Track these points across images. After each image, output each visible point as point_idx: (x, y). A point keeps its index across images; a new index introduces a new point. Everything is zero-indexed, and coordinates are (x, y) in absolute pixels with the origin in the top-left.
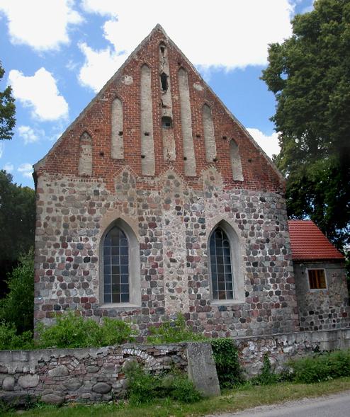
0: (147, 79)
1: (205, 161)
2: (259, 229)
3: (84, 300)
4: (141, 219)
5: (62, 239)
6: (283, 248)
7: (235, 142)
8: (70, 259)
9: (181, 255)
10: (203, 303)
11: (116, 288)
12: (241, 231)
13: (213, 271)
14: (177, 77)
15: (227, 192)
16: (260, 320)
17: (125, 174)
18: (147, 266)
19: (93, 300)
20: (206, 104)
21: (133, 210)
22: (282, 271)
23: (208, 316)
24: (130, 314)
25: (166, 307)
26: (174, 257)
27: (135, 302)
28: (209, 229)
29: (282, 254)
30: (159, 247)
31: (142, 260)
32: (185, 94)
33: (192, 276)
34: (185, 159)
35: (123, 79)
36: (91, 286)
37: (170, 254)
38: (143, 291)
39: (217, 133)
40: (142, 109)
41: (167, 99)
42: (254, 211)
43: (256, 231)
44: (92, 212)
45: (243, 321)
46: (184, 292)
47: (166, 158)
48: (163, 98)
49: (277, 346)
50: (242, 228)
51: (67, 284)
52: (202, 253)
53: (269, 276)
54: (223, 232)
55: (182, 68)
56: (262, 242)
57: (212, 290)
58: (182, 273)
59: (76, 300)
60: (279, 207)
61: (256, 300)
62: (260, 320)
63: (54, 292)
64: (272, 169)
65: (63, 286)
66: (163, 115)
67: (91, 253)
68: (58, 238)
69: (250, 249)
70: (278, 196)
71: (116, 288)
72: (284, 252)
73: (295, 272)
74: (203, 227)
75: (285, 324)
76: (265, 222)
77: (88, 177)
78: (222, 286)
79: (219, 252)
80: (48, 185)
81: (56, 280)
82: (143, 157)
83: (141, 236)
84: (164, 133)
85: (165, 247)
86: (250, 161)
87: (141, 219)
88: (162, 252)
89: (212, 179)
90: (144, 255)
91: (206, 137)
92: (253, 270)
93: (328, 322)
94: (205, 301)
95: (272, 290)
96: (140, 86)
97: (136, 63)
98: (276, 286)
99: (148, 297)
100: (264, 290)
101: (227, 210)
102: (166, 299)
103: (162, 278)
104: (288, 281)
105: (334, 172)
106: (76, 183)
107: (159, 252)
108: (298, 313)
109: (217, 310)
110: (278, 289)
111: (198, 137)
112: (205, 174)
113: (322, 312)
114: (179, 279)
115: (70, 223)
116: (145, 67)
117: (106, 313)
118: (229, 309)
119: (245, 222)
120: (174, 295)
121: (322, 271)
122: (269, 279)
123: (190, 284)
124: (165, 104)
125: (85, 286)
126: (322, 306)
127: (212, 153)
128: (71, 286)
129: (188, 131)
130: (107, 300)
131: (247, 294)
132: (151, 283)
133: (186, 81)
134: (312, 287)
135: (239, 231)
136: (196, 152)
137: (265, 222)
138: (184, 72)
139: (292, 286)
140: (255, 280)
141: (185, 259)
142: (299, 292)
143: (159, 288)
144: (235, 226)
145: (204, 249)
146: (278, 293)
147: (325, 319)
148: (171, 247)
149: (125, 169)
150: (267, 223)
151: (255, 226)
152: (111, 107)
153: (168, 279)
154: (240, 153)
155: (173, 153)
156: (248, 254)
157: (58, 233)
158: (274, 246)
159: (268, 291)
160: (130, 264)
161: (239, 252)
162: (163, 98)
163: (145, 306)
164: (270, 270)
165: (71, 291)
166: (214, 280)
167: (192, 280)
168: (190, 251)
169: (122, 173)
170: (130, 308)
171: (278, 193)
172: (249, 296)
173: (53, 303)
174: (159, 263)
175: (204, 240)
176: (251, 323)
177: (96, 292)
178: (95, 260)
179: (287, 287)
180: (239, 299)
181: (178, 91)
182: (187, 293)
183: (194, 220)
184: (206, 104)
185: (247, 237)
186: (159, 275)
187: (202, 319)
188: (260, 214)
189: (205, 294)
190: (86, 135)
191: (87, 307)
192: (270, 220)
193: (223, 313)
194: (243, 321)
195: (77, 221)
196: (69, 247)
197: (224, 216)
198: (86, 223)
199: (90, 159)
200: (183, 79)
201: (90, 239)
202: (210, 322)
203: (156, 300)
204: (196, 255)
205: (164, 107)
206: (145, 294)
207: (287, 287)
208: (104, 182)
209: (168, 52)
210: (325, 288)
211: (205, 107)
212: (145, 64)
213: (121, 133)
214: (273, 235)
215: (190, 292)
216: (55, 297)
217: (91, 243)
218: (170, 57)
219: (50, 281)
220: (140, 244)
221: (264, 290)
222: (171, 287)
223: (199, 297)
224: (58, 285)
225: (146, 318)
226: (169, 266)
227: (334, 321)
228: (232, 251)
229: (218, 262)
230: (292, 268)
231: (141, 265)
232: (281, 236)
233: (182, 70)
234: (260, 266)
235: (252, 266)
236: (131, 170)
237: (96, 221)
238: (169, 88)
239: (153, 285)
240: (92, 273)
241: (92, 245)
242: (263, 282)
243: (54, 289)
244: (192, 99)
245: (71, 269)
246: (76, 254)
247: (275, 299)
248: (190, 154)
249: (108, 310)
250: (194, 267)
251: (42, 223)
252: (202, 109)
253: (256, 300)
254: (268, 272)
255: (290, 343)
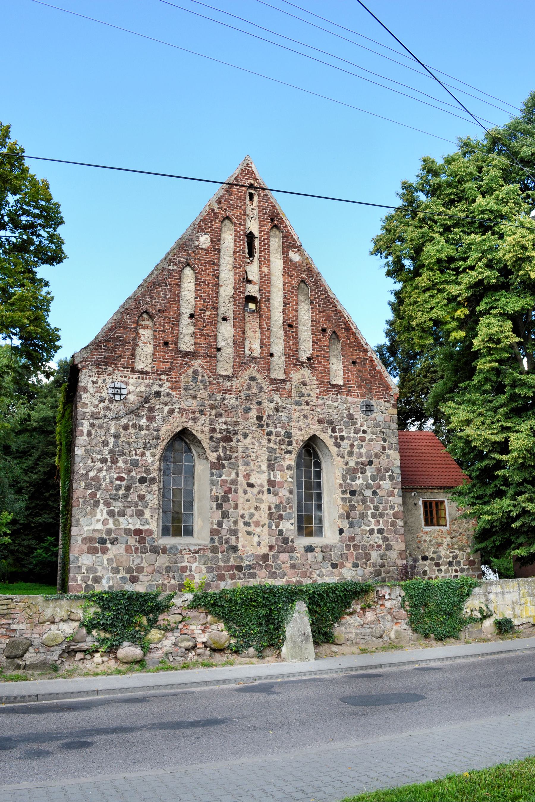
0: (228, 239)
1: (297, 360)
2: (360, 447)
3: (138, 532)
4: (213, 430)
5: (111, 452)
6: (390, 473)
7: (337, 337)
8: (121, 479)
9: (260, 479)
10: (286, 541)
11: (177, 519)
12: (336, 449)
13: (299, 499)
14: (268, 240)
15: (322, 399)
16: (356, 566)
17: (195, 372)
18: (219, 492)
19: (150, 532)
20: (303, 281)
21: (203, 419)
22: (387, 502)
23: (291, 558)
24: (195, 552)
25: (240, 546)
26: (252, 480)
27: (201, 536)
28: (296, 447)
29: (388, 481)
30: (234, 467)
31: (212, 483)
32: (277, 263)
33: (273, 506)
34: (272, 355)
35: (197, 239)
36: (147, 513)
37: (247, 476)
38: (212, 523)
39: (314, 322)
40: (220, 284)
41: (253, 271)
42: (354, 424)
43: (355, 450)
44: (151, 419)
45: (334, 566)
46: (263, 526)
47: (247, 352)
48: (248, 268)
49: (378, 599)
50: (338, 446)
51: (116, 510)
52: (287, 477)
53: (370, 508)
54: (314, 449)
55: (275, 226)
56: (362, 464)
57: (296, 525)
58: (261, 501)
59: (127, 532)
60: (388, 419)
61: (352, 539)
62: (356, 566)
63: (98, 521)
64: (382, 376)
65: (111, 514)
66: (247, 294)
67: (147, 471)
68: (106, 450)
69: (347, 473)
70: (387, 405)
71: (177, 519)
72: (391, 478)
73: (404, 504)
74: (290, 444)
75: (389, 573)
76: (368, 438)
77: (147, 373)
78: (308, 524)
79: (308, 475)
80: (94, 383)
81: (102, 506)
82: (219, 350)
83: (213, 452)
84: (247, 319)
85: (241, 468)
86: (354, 363)
87: (213, 430)
88: (237, 474)
89: (304, 384)
90: (215, 477)
91: (300, 327)
92: (350, 500)
93: (447, 571)
94: (288, 538)
95: (373, 526)
96: (219, 250)
97: (216, 215)
98: (378, 522)
99: (218, 530)
100: (364, 527)
101: (320, 422)
102: (240, 535)
103: (236, 507)
104: (395, 516)
105: (478, 358)
106: (131, 381)
107: (234, 473)
108: (406, 558)
109: (303, 550)
110: (381, 526)
111: (290, 326)
112: (296, 376)
113: (440, 557)
114: (257, 508)
115: (122, 432)
116: (227, 221)
117: (165, 551)
118: (317, 549)
119: (342, 438)
120: (249, 529)
121: (442, 502)
122: (369, 512)
123: (271, 515)
124: (250, 277)
125: (140, 514)
126: (440, 549)
127: (306, 350)
128: (122, 514)
129: (277, 317)
130: (165, 532)
131: (341, 531)
132: (223, 512)
133: (279, 246)
134: (427, 524)
135: (334, 450)
136: (286, 347)
137: (368, 438)
138: (277, 233)
139: (400, 523)
140: (352, 513)
141: (265, 484)
142: (409, 528)
143: (233, 520)
144: (330, 443)
145: (289, 472)
146: (380, 531)
147: (443, 568)
148: (248, 468)
149: (196, 363)
150: (371, 440)
151: (356, 443)
152: (180, 279)
153: (244, 509)
154: (343, 351)
155: (256, 346)
156: (344, 480)
157: (105, 443)
158: (378, 470)
159: (368, 528)
160: (196, 487)
161: (332, 473)
162: (248, 268)
163: (214, 542)
164: (372, 501)
165: (121, 519)
166: (300, 509)
167: (273, 510)
168: (272, 473)
169: (191, 370)
170: (195, 545)
171: (388, 401)
172: (343, 534)
173: (97, 535)
174: (233, 488)
175: (290, 460)
176: (344, 570)
177: (152, 523)
178: (153, 480)
179: (393, 524)
180: (329, 536)
181: (269, 260)
182: (266, 527)
183: (278, 434)
184: (303, 281)
185: (344, 458)
186: (232, 503)
187: (284, 562)
188: (362, 428)
189: (288, 530)
190: (145, 316)
191: (142, 541)
192: (374, 437)
193: (309, 555)
194: (334, 566)
195: (132, 430)
196: (120, 464)
197: (316, 429)
198: (143, 432)
199: (149, 349)
200: (276, 243)
201: (148, 453)
202: (293, 566)
203: (228, 536)
204: (279, 479)
205: (249, 282)
206: (215, 527)
207: (393, 524)
208: (168, 381)
209: (259, 202)
210: (446, 525)
211: (302, 285)
212: (227, 218)
213: (192, 316)
214: (377, 456)
215: (270, 527)
216: (99, 526)
217: (150, 459)
218: (261, 209)
219: (94, 506)
220: (211, 462)
221: (364, 527)
222: (247, 520)
223: (281, 533)
224: (105, 512)
225: (214, 558)
226: (245, 492)
227: (456, 571)
228: (324, 475)
229: (306, 488)
230: (401, 499)
231: (212, 490)
232: (388, 456)
233: (275, 229)
234: (359, 495)
235: (348, 495)
236: (202, 367)
237: (155, 431)
238: (257, 256)
239: (225, 515)
240: (148, 497)
241: (150, 461)
242: (362, 516)
243: (99, 516)
244: (286, 273)
245: (122, 492)
246: (128, 472)
247: (377, 539)
248: (278, 348)
249: (168, 547)
250: (276, 494)
251: (85, 432)
252: (298, 288)
253: (352, 539)
254: (369, 503)
255: (393, 596)
